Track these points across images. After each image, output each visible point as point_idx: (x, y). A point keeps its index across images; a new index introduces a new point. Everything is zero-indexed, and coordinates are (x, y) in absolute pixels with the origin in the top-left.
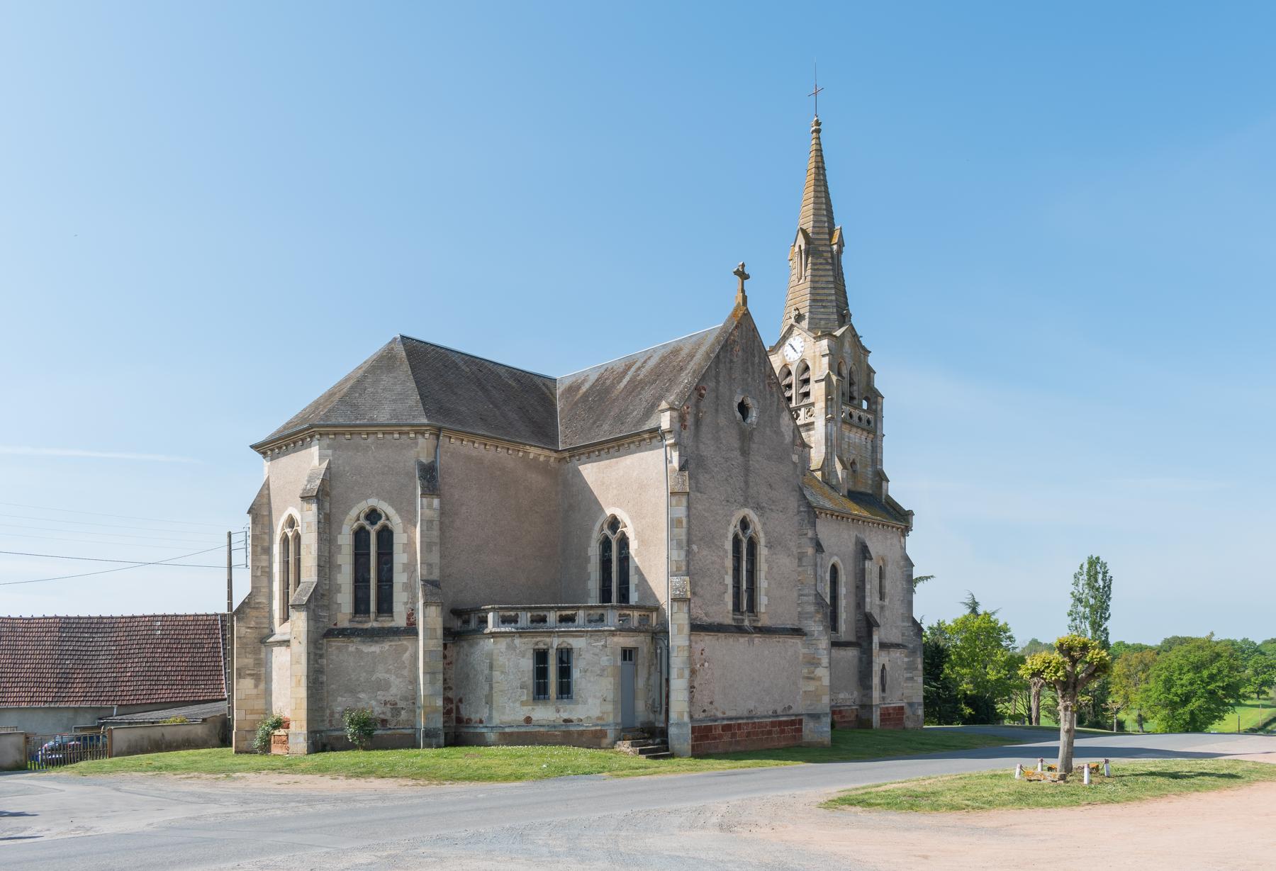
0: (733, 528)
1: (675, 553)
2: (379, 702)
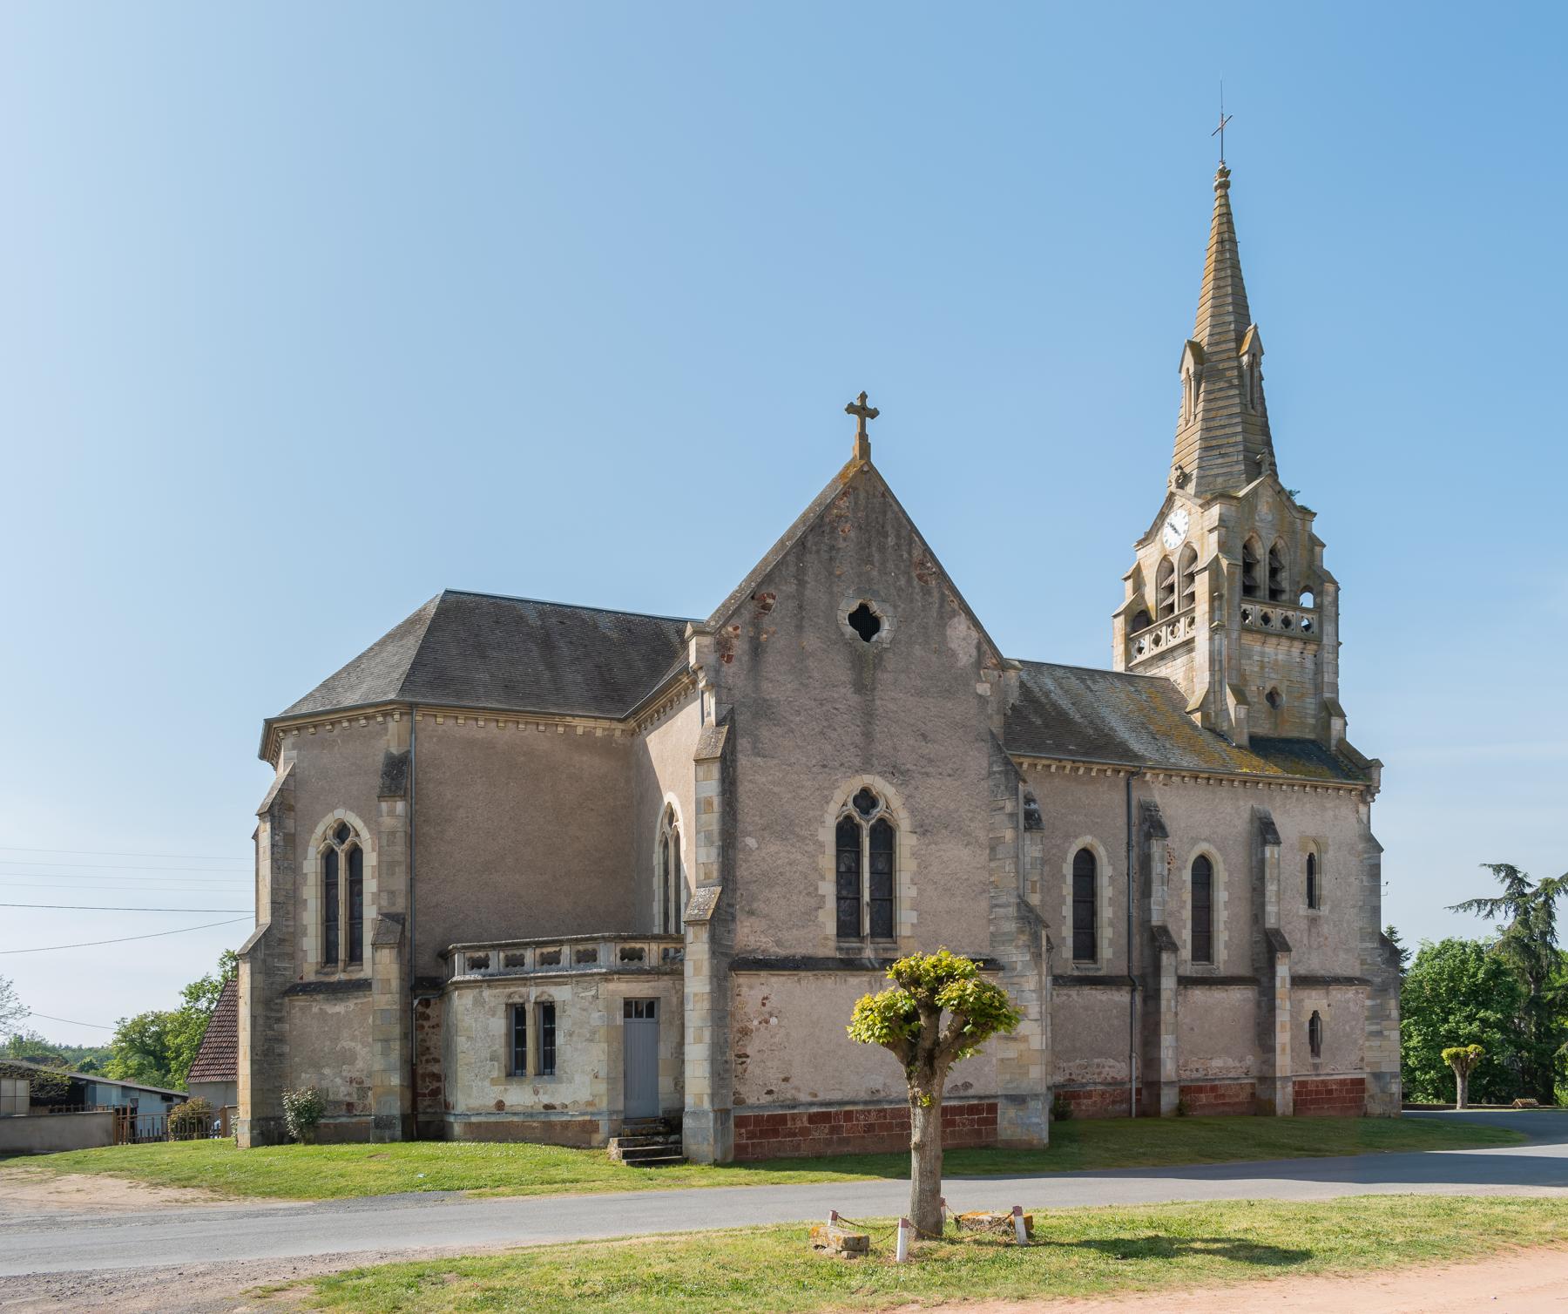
0: (839, 802)
1: (703, 851)
2: (343, 1078)
